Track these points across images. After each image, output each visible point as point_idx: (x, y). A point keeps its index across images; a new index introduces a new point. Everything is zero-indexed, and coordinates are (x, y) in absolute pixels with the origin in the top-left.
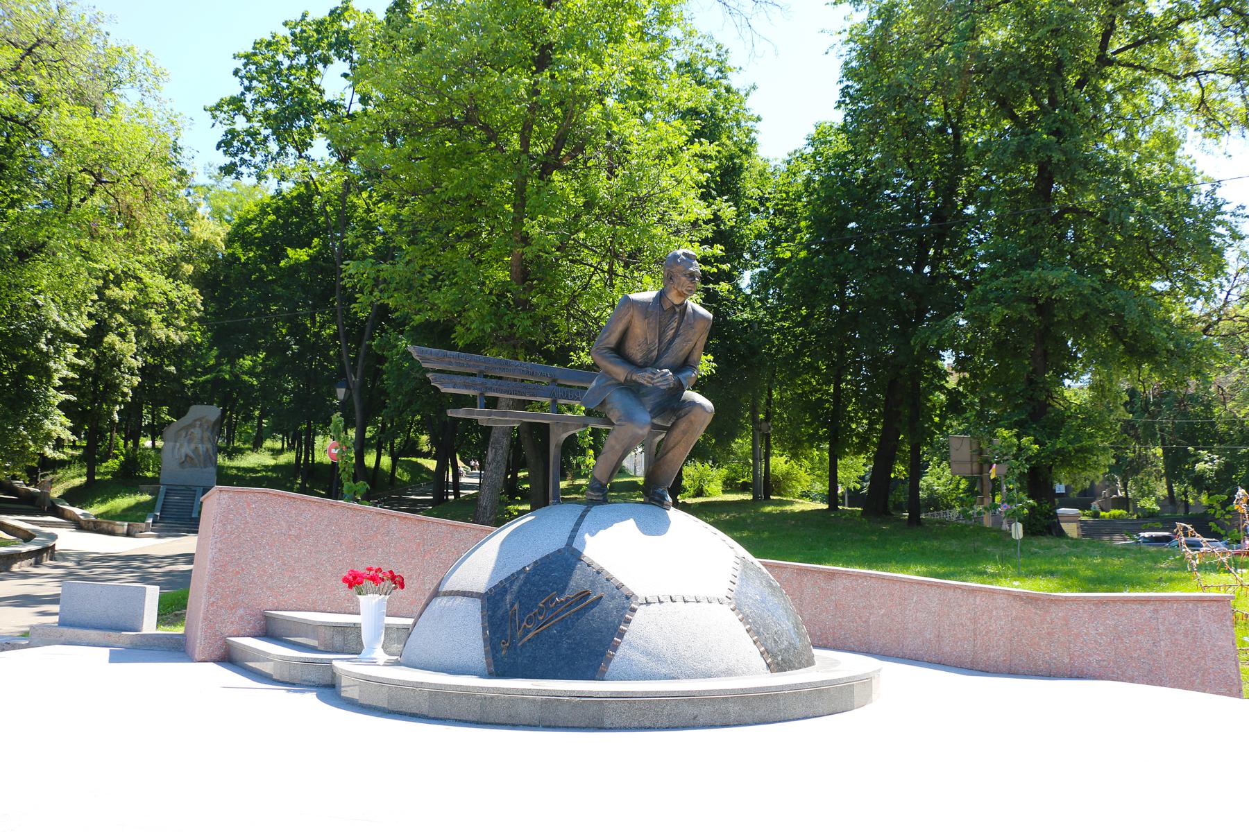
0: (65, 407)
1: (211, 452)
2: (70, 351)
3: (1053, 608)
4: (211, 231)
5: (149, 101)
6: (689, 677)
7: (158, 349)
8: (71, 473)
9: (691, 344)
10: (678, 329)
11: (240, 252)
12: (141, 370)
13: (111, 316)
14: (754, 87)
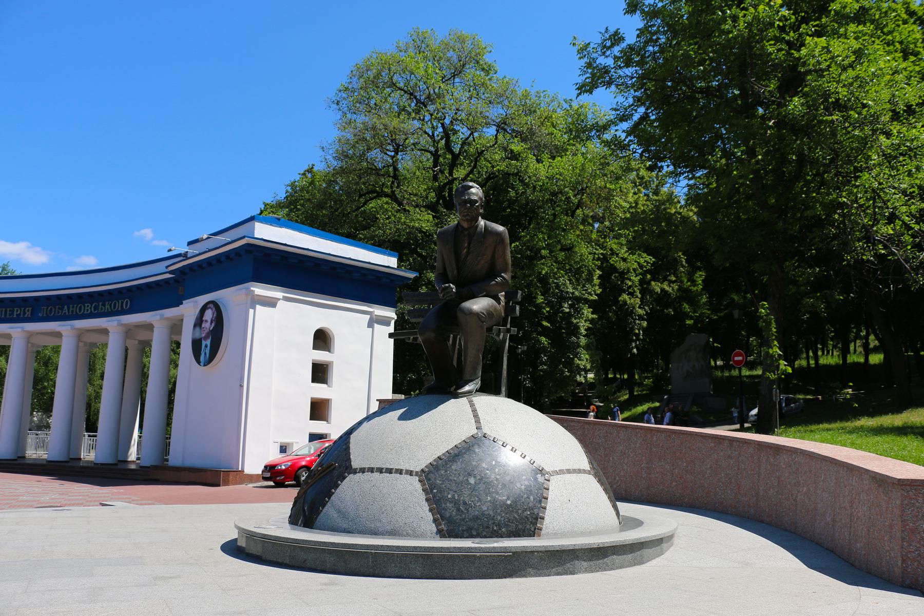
2: (587, 312)
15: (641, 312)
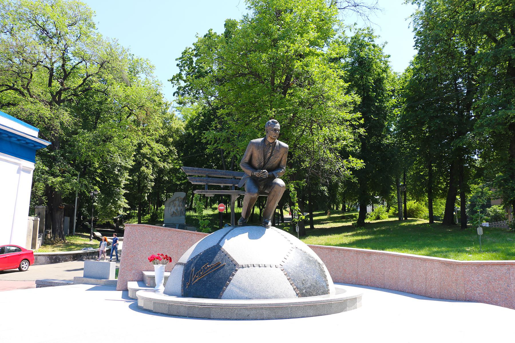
0: (125, 195)
1: (183, 210)
2: (126, 175)
3: (458, 268)
4: (179, 123)
5: (149, 78)
6: (257, 298)
7: (161, 172)
8: (134, 220)
9: (279, 159)
10: (272, 152)
11: (191, 131)
12: (155, 179)
13: (143, 160)
14: (386, 43)
15: (152, 177)
